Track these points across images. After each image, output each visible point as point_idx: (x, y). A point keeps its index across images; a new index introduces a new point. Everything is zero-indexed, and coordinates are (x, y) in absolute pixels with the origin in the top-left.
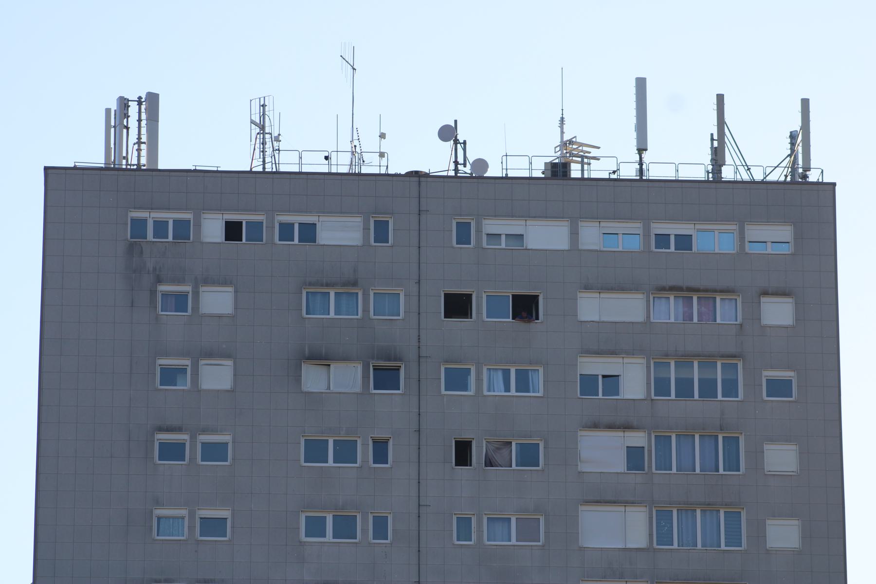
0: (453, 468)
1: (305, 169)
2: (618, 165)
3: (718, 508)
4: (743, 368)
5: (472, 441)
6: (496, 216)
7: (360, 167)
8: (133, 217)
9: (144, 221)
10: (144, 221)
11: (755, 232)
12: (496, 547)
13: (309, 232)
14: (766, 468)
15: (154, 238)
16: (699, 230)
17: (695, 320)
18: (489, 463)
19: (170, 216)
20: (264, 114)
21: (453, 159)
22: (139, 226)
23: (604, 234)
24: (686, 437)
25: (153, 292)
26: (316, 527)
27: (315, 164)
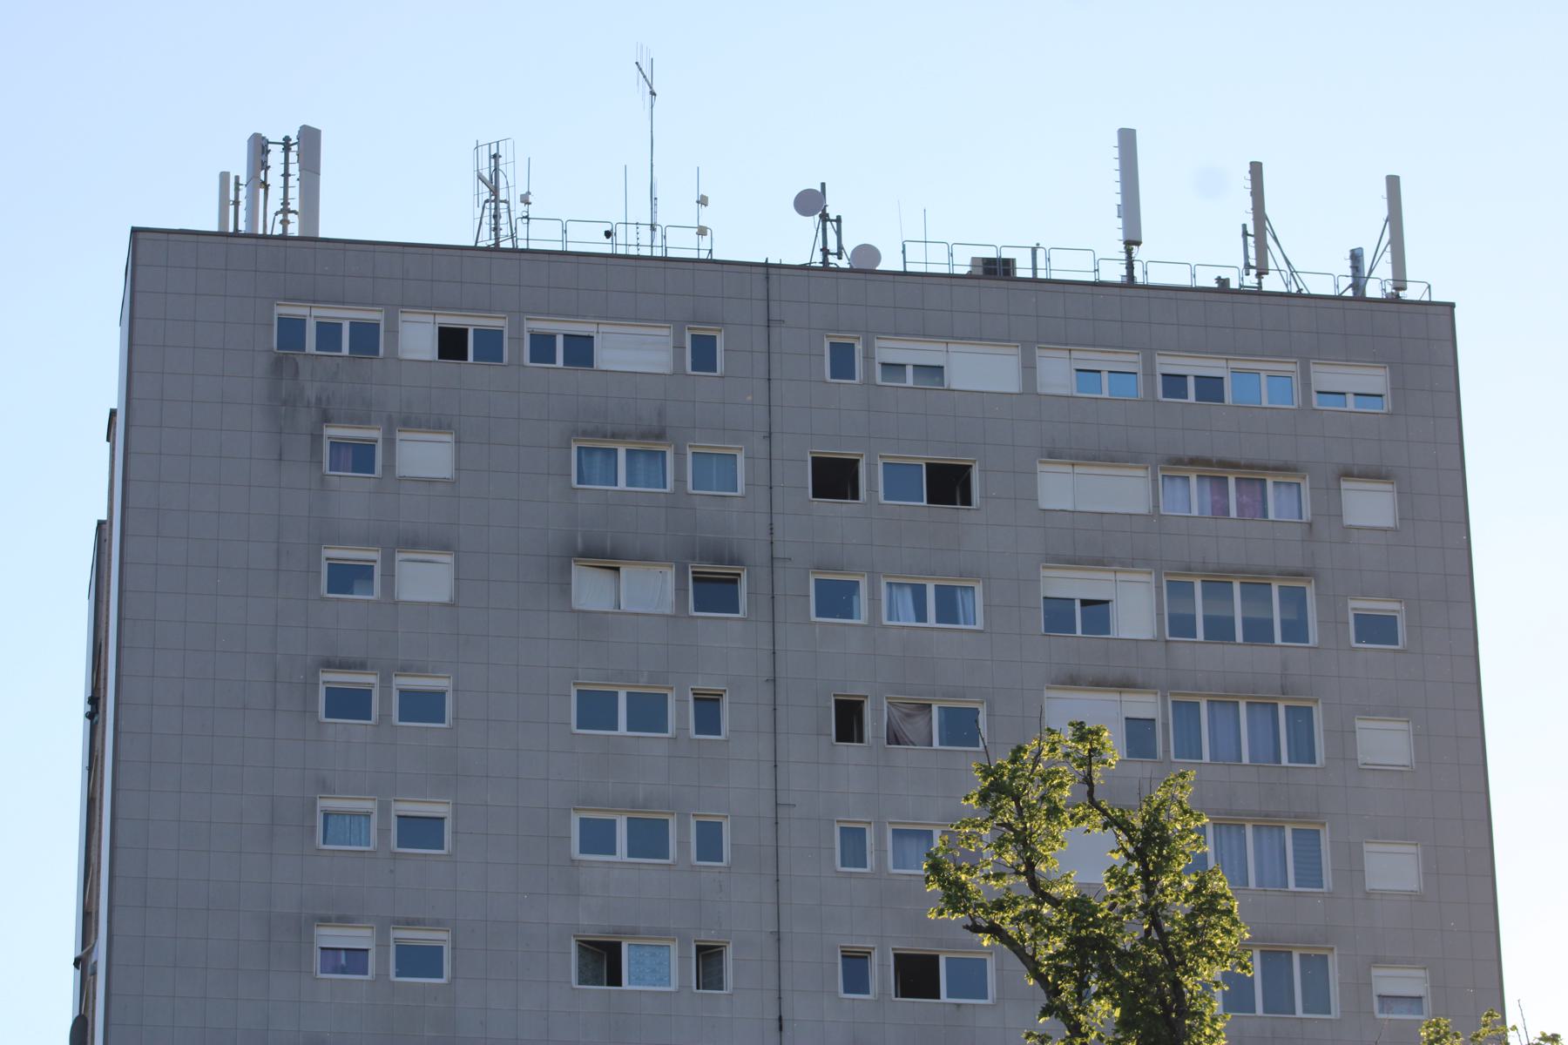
0: (832, 743)
1: (572, 248)
2: (1096, 262)
3: (1280, 821)
4: (1316, 594)
5: (863, 701)
6: (898, 333)
7: (666, 250)
8: (281, 315)
9: (300, 323)
10: (300, 323)
11: (1327, 376)
12: (908, 878)
13: (581, 351)
14: (1362, 758)
15: (317, 350)
16: (1234, 372)
17: (1233, 513)
18: (895, 738)
19: (345, 315)
20: (496, 170)
21: (819, 245)
22: (291, 331)
23: (1078, 370)
24: (1224, 704)
25: (316, 438)
26: (598, 837)
27: (587, 240)
